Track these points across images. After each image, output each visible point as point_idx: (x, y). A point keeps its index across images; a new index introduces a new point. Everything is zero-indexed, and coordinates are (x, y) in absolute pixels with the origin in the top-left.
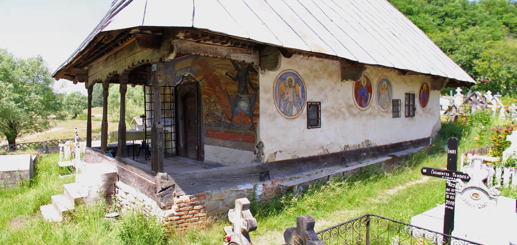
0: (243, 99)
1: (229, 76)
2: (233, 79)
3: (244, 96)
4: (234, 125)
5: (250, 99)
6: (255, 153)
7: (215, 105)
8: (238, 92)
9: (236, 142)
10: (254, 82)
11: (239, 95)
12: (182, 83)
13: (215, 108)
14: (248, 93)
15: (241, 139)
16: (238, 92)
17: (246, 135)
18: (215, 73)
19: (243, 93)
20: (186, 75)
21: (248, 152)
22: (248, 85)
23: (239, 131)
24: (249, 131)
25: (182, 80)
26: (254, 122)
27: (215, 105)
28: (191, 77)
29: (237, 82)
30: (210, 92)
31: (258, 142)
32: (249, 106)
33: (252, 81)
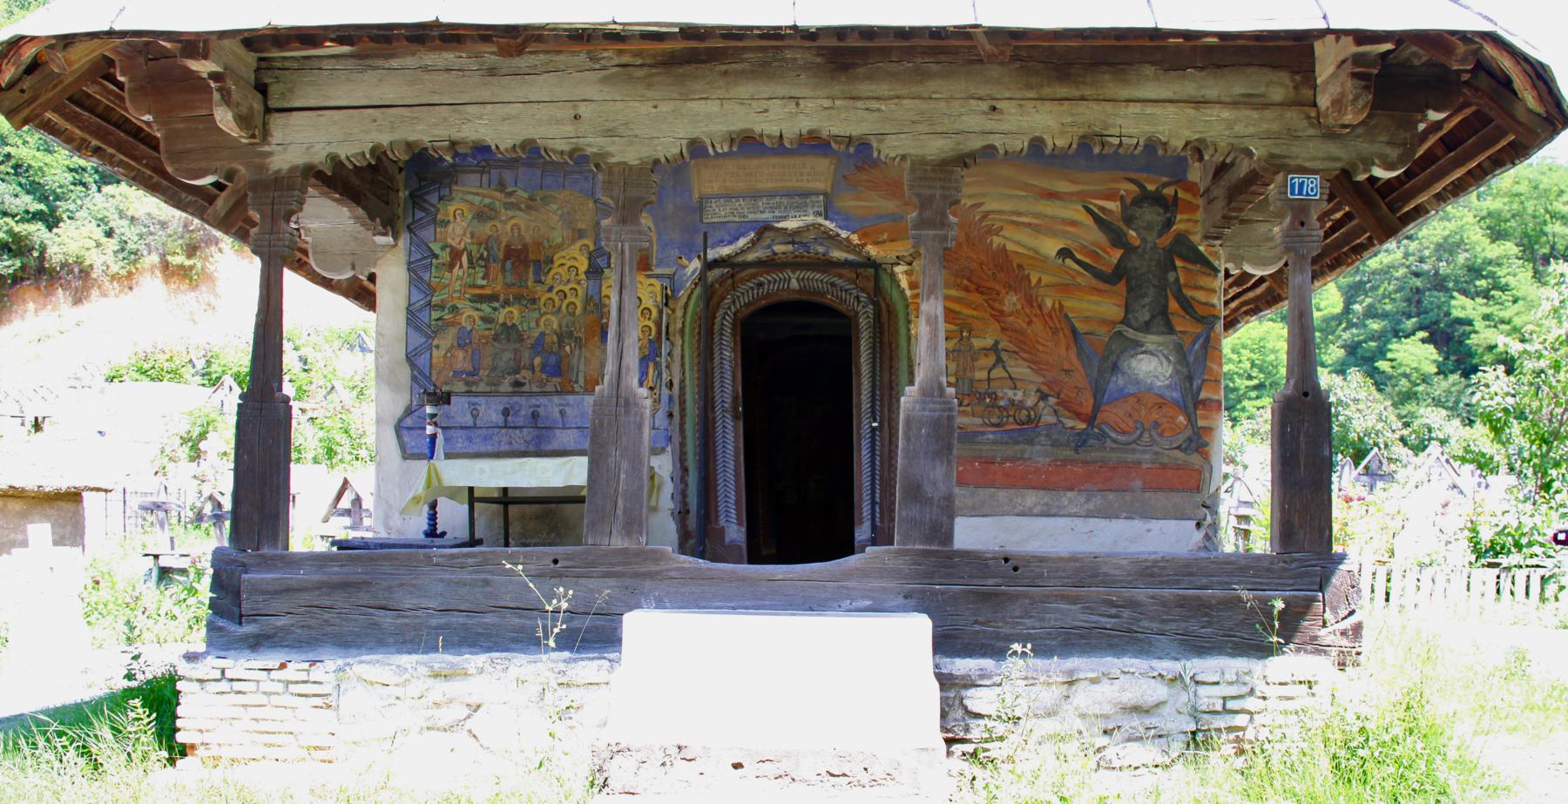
0: (1151, 347)
1: (1078, 262)
2: (1097, 274)
3: (1151, 341)
4: (1103, 436)
5: (1181, 352)
6: (1198, 525)
7: (999, 360)
8: (1125, 321)
9: (1111, 496)
10: (1200, 296)
11: (1130, 333)
12: (751, 257)
13: (998, 373)
14: (1170, 330)
15: (1138, 484)
16: (1125, 321)
17: (1164, 467)
18: (997, 241)
19: (1146, 328)
20: (791, 225)
21: (1173, 522)
22: (1173, 305)
23: (1130, 457)
24: (1178, 454)
25: (754, 243)
26: (1201, 423)
27: (999, 360)
28: (832, 238)
29: (1121, 287)
30: (966, 311)
31: (1212, 490)
32: (1177, 372)
33: (1188, 293)
